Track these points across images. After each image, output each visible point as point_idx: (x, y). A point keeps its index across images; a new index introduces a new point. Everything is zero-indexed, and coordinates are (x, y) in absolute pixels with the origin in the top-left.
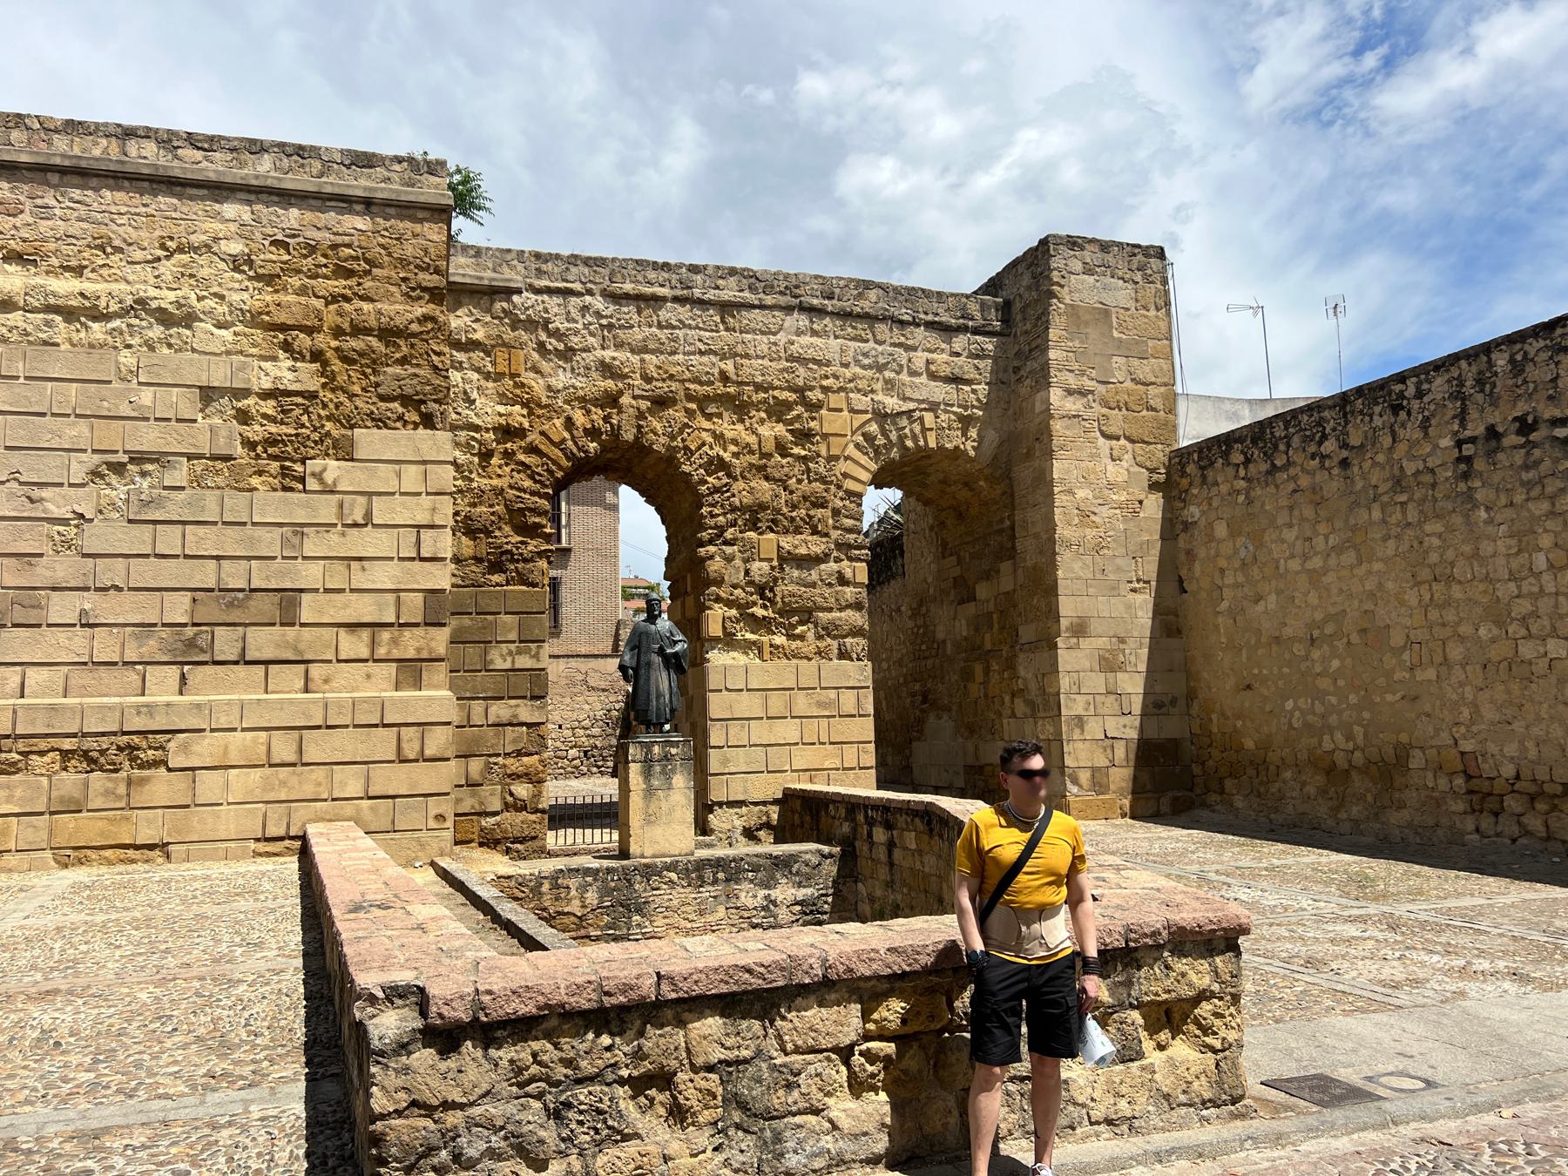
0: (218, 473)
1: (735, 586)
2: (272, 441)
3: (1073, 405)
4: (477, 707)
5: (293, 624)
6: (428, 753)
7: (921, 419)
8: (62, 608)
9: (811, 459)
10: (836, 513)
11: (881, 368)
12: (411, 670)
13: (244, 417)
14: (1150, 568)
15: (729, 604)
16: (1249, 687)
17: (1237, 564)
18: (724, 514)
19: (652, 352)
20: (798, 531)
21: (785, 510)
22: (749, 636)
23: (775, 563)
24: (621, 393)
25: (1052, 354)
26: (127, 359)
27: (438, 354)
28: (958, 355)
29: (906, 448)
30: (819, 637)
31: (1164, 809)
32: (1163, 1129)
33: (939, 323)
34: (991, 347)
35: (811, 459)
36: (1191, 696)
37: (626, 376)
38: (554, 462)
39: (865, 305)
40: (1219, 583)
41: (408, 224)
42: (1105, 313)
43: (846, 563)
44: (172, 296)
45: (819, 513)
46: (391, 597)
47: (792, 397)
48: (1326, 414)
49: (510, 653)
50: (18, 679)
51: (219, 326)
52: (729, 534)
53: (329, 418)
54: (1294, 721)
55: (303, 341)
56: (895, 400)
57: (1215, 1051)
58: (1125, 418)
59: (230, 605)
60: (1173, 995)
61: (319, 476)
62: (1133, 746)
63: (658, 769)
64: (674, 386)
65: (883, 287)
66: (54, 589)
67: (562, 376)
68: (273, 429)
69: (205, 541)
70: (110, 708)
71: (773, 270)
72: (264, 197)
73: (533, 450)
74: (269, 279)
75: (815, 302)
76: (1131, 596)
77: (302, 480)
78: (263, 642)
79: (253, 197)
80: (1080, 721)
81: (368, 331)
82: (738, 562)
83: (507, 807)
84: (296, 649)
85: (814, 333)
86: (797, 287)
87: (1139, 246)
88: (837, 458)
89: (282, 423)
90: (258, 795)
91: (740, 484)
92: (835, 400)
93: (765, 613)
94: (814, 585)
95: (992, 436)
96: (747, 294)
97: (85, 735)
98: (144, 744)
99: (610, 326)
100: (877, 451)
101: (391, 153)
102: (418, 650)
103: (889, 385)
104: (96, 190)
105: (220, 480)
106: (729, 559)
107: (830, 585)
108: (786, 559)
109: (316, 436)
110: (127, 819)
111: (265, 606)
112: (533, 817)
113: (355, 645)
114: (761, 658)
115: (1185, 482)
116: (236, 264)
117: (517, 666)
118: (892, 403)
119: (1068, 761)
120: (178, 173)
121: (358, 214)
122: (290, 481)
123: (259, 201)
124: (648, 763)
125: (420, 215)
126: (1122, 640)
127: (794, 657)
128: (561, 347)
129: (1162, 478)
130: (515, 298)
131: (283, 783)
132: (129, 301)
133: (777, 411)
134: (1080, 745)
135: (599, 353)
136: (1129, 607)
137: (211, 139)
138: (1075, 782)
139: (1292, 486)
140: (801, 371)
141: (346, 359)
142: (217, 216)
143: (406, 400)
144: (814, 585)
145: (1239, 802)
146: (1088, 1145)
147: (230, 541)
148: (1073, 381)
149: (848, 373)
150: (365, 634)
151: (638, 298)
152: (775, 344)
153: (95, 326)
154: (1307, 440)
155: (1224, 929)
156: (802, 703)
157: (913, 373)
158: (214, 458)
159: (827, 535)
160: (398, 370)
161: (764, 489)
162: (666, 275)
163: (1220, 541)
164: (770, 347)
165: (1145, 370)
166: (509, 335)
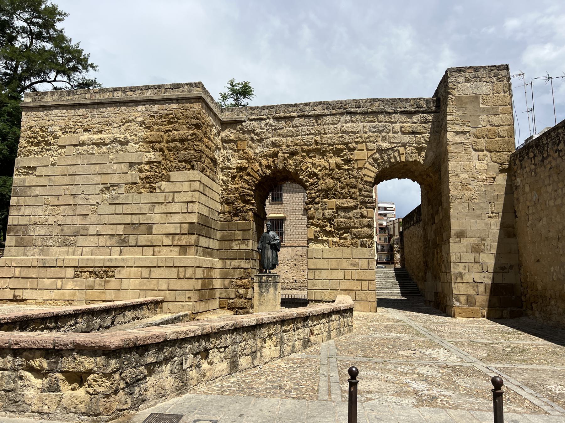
0: (132, 188)
1: (319, 219)
2: (147, 178)
3: (458, 139)
4: (228, 262)
5: (151, 234)
6: (187, 276)
7: (398, 150)
8: (92, 230)
9: (351, 170)
10: (360, 190)
11: (380, 132)
12: (184, 249)
13: (140, 171)
14: (499, 207)
15: (317, 226)
16: (538, 261)
17: (533, 204)
18: (315, 193)
19: (290, 136)
20: (344, 197)
21: (339, 190)
22: (325, 238)
23: (335, 210)
24: (278, 152)
25: (448, 118)
26: (111, 156)
27: (196, 145)
28: (415, 123)
29: (392, 163)
30: (353, 238)
31: (505, 315)
32: (61, 420)
33: (406, 111)
34: (431, 118)
35: (351, 170)
36: (520, 266)
37: (281, 146)
38: (255, 178)
39: (374, 108)
40: (527, 213)
41: (189, 105)
42: (476, 97)
43: (365, 209)
44: (123, 136)
45: (353, 190)
46: (179, 225)
47: (342, 147)
48: (560, 131)
49: (239, 244)
50: (81, 251)
51: (135, 144)
52: (316, 200)
53: (164, 169)
54: (554, 277)
55: (157, 145)
56: (387, 144)
57: (91, 395)
58: (486, 142)
59: (134, 228)
60: (76, 370)
61: (159, 187)
62: (489, 287)
63: (264, 285)
64: (297, 147)
65: (382, 100)
66: (91, 224)
67: (259, 149)
68: (148, 174)
69: (128, 209)
70: (101, 259)
71: (336, 100)
72: (148, 103)
73: (248, 174)
74: (149, 128)
75: (353, 110)
76: (488, 220)
77: (155, 189)
78: (143, 240)
79: (145, 103)
80: (461, 275)
81: (176, 141)
82: (320, 210)
83: (237, 296)
84: (151, 242)
85: (353, 122)
86: (345, 105)
87: (495, 66)
88: (361, 169)
89: (151, 172)
90: (138, 287)
91: (322, 181)
92: (360, 146)
93: (330, 229)
94: (350, 218)
95: (431, 154)
96: (325, 111)
97: (95, 267)
98: (109, 271)
99: (275, 129)
100: (379, 165)
101: (184, 83)
102: (186, 242)
103: (384, 139)
104: (106, 108)
105: (133, 190)
106: (317, 209)
107: (357, 218)
108: (339, 208)
109: (160, 175)
110: (104, 292)
111: (143, 228)
112: (245, 301)
113: (167, 241)
114: (329, 246)
115: (515, 167)
116: (141, 124)
117: (241, 248)
118: (385, 145)
119: (455, 292)
120: (126, 99)
121: (175, 104)
122: (152, 190)
123: (147, 104)
124: (260, 283)
125: (193, 101)
126: (483, 239)
127: (342, 246)
128: (259, 138)
129: (506, 167)
130: (244, 124)
131: (145, 284)
132: (112, 139)
133: (337, 153)
134: (461, 284)
135: (272, 139)
136: (487, 224)
137: (135, 88)
138: (458, 300)
139: (549, 166)
140: (347, 136)
141: (169, 150)
142: (136, 111)
143: (187, 161)
144: (350, 218)
145: (537, 315)
146: (28, 419)
147: (134, 209)
148: (458, 128)
149: (366, 135)
150: (171, 237)
151: (285, 118)
152: (336, 128)
153: (104, 147)
154: (554, 143)
155: (98, 346)
156: (345, 264)
157: (395, 132)
158: (132, 184)
159: (356, 199)
160: (184, 152)
161: (330, 182)
162: (295, 108)
163: (527, 194)
164: (332, 130)
165: (497, 120)
166: (242, 136)
